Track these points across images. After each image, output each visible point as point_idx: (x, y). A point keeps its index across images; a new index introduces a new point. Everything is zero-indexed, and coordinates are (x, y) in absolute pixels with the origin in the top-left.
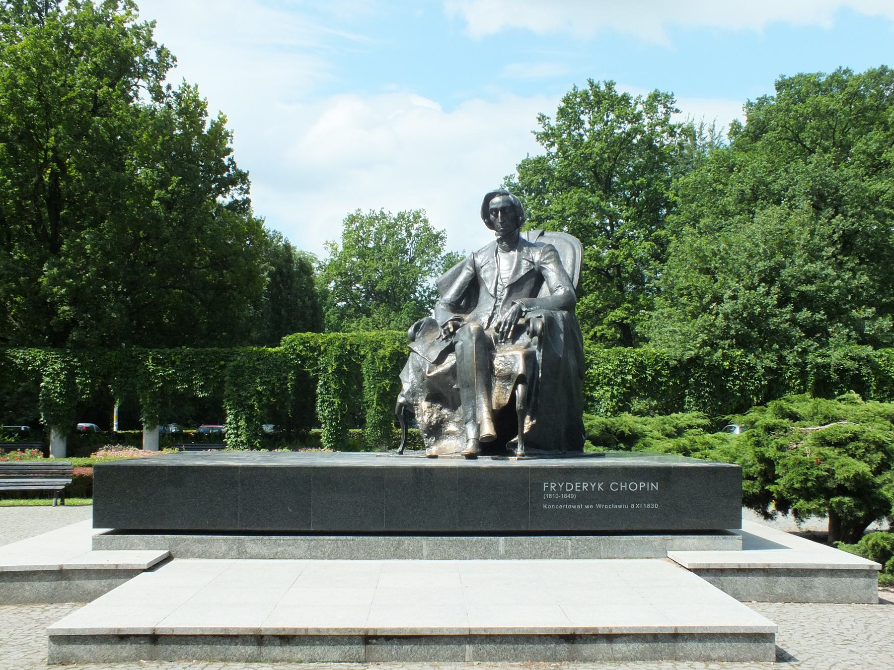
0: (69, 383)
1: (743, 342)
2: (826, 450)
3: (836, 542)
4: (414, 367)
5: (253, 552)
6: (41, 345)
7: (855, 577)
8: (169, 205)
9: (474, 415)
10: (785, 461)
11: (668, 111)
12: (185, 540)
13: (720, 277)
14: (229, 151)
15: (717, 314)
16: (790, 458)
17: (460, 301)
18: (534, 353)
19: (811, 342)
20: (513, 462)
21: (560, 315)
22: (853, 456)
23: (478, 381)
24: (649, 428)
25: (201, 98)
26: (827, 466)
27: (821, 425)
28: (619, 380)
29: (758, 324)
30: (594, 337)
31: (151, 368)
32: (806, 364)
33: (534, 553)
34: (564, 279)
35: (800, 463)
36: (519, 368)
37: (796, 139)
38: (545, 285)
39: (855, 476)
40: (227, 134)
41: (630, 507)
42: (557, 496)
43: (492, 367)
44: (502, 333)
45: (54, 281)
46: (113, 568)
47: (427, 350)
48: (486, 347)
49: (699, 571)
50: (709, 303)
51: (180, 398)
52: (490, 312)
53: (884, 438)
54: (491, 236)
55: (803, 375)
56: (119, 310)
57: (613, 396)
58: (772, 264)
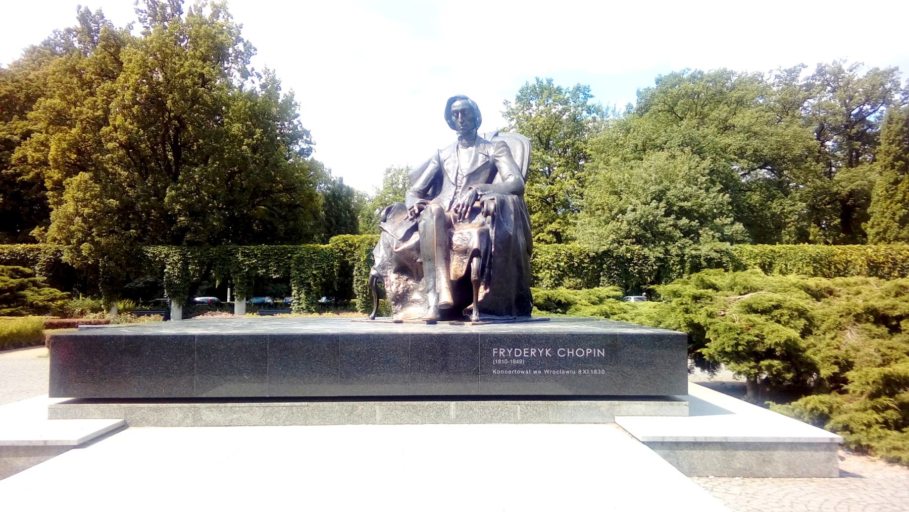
0: (184, 269)
1: (639, 240)
2: (753, 317)
3: (767, 402)
4: (384, 244)
5: (208, 420)
6: (167, 244)
7: (817, 450)
8: (254, 149)
9: (435, 285)
10: (716, 327)
11: (587, 96)
12: (141, 408)
13: (624, 197)
14: (298, 116)
15: (622, 222)
16: (720, 324)
17: (427, 189)
18: (488, 231)
19: (687, 240)
20: (472, 327)
21: (511, 199)
22: (779, 322)
23: (439, 255)
24: (578, 297)
25: (277, 78)
26: (757, 332)
27: (741, 294)
28: (555, 266)
29: (651, 229)
30: (539, 239)
31: (241, 259)
32: (684, 255)
33: (484, 417)
34: (514, 169)
35: (730, 329)
36: (474, 243)
37: (671, 110)
38: (498, 175)
39: (786, 342)
40: (296, 104)
41: (577, 373)
42: (506, 362)
43: (451, 243)
44: (461, 214)
45: (174, 200)
46: (42, 444)
47: (396, 229)
48: (446, 226)
49: (652, 445)
50: (617, 214)
51: (259, 279)
52: (451, 198)
53: (806, 306)
54: (453, 136)
55: (682, 262)
56: (219, 220)
57: (551, 277)
58: (660, 188)
